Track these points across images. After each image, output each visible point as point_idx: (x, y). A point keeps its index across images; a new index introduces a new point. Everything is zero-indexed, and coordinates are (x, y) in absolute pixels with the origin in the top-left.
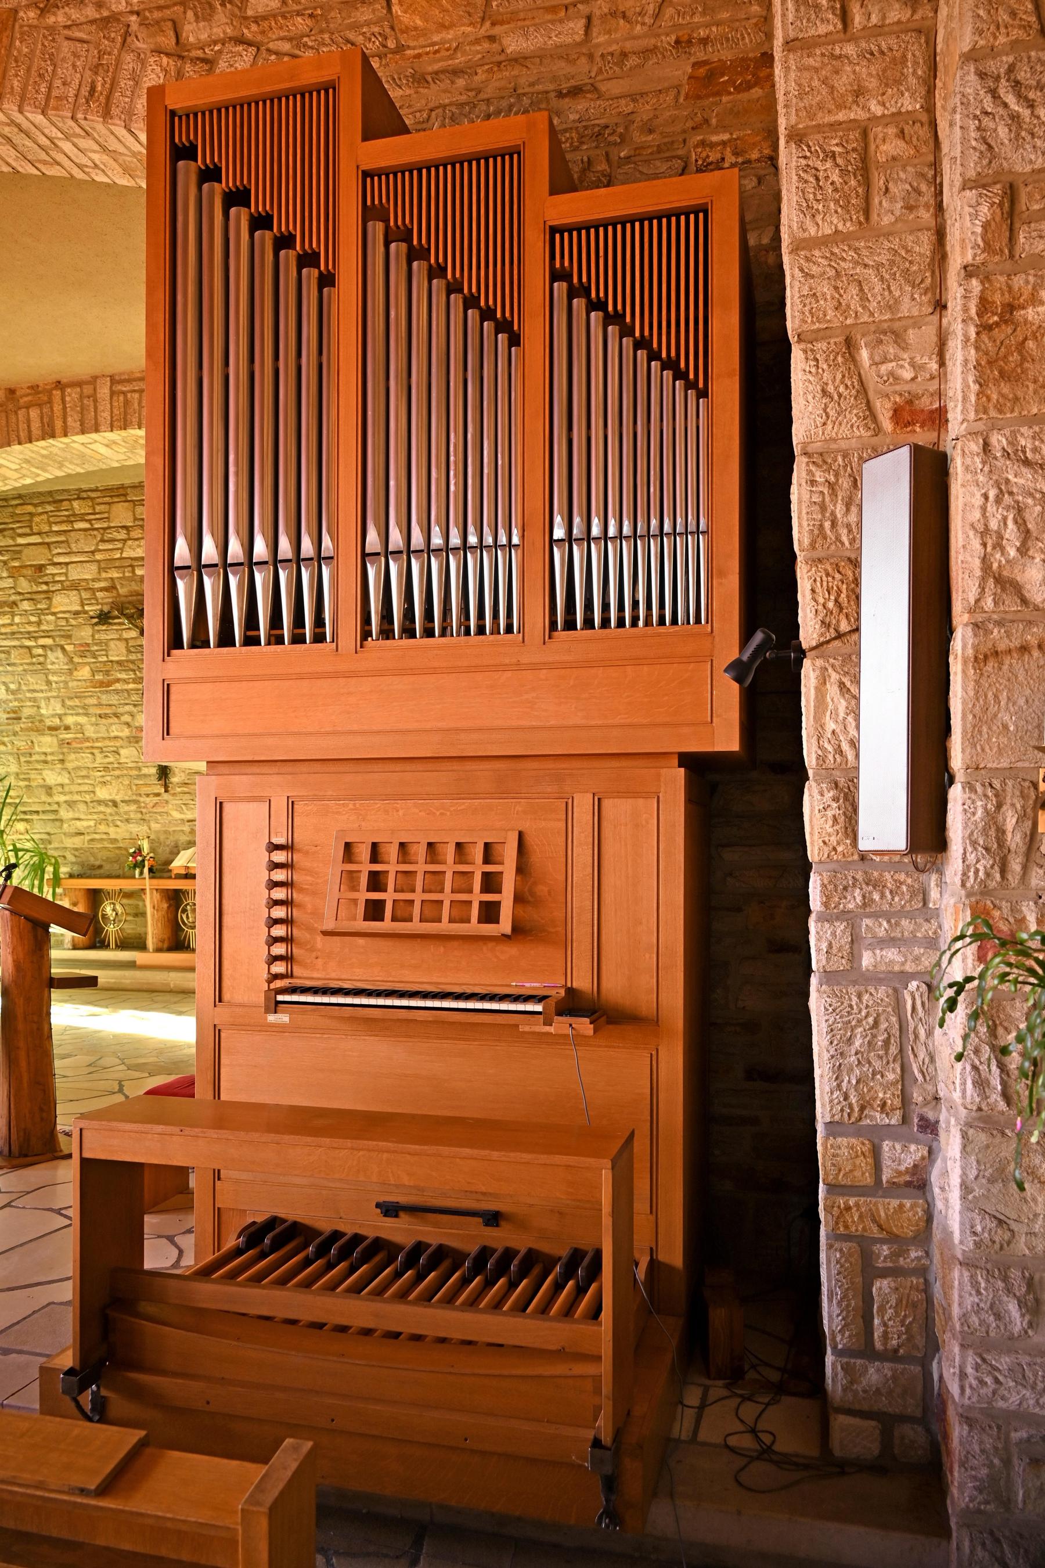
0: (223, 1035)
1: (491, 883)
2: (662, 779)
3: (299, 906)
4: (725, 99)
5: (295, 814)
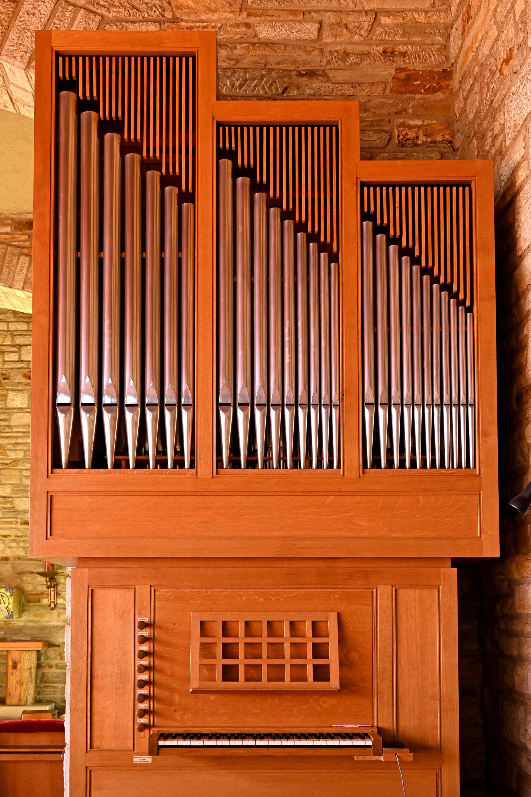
0: (92, 774)
1: (320, 651)
2: (442, 576)
4: (417, 96)
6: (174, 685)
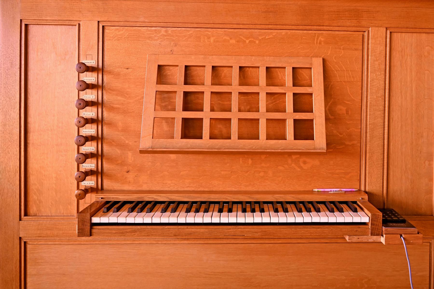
0: (28, 246)
1: (302, 103)
3: (110, 124)
5: (106, 38)
6: (127, 142)
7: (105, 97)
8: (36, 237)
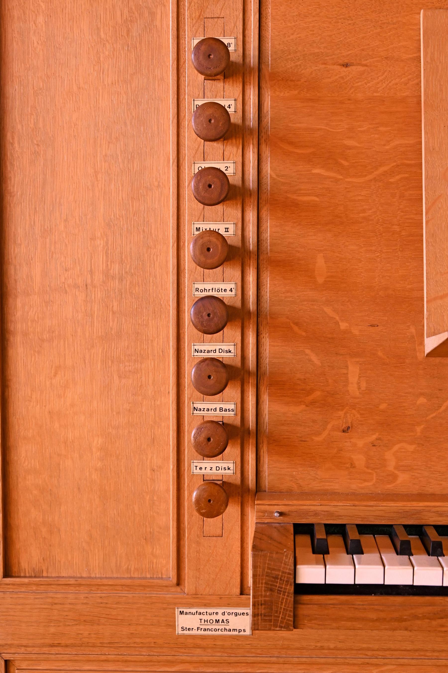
6: (343, 326)
7: (267, 169)
8: (43, 645)
